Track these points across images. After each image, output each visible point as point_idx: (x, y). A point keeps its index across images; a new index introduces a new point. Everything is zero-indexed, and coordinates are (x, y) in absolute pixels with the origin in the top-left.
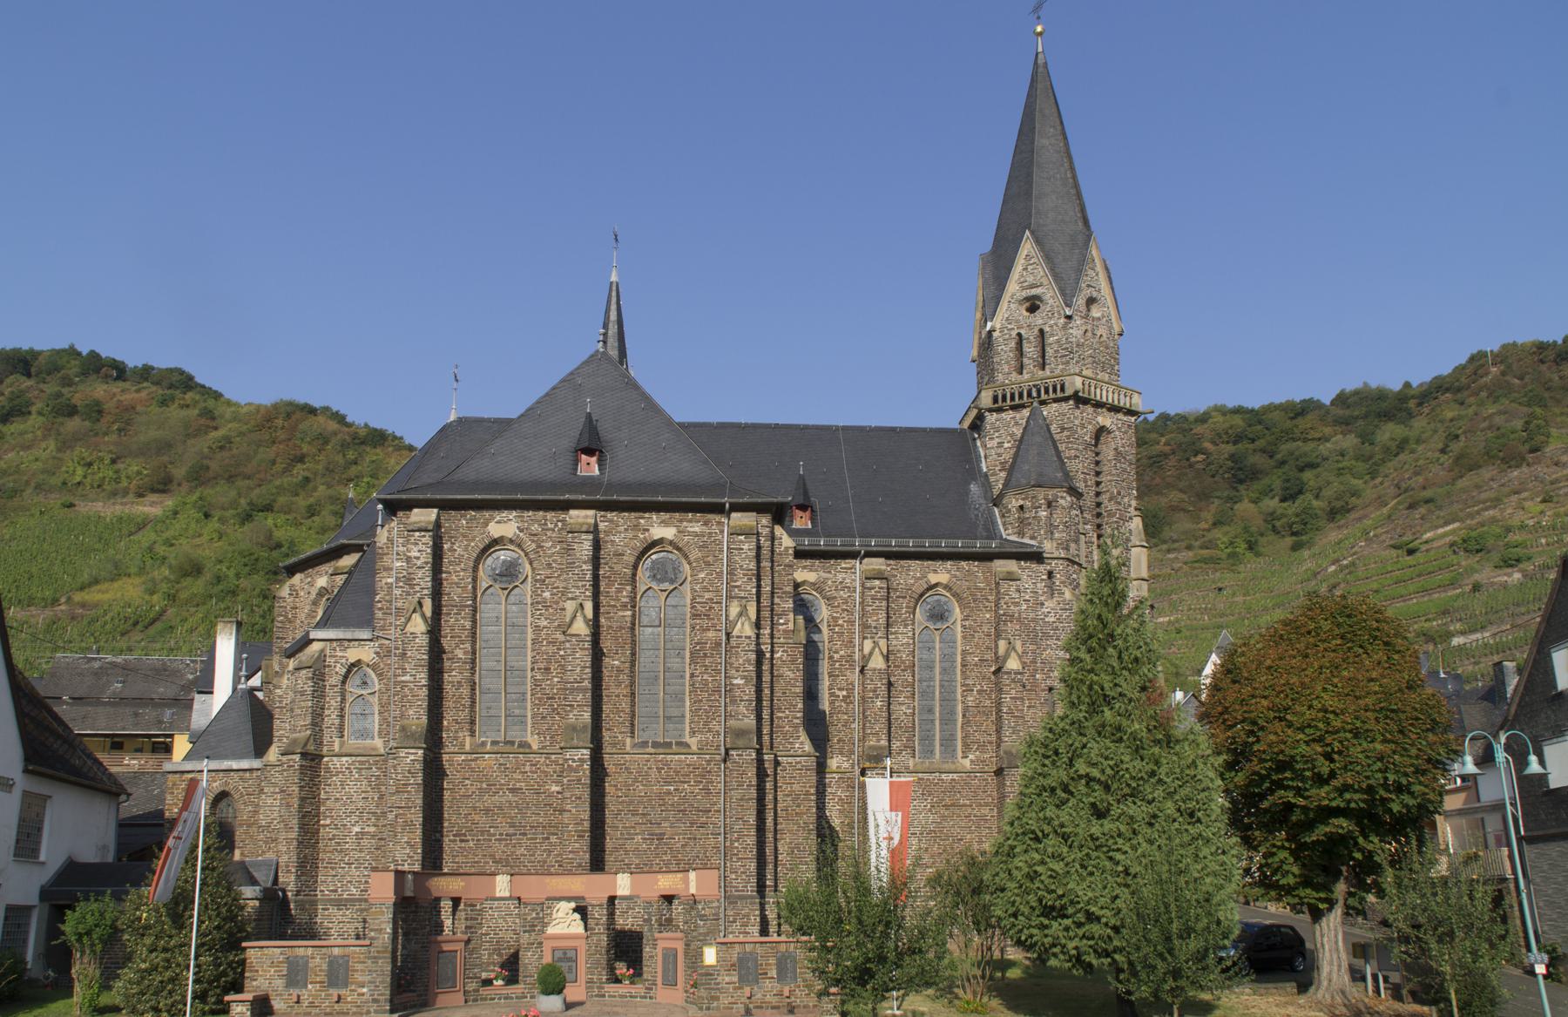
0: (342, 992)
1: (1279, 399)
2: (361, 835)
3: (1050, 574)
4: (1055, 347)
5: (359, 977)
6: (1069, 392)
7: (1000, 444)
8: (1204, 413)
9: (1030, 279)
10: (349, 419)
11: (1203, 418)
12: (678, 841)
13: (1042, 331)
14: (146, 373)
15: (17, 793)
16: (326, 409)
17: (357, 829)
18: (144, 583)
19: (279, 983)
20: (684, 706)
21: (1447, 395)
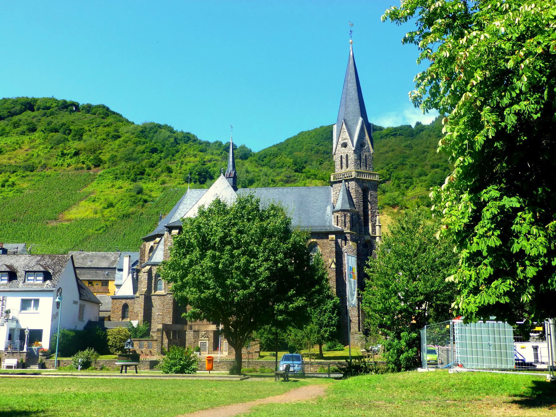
2: (159, 315)
10: (175, 129)
13: (347, 155)
14: (89, 109)
15: (78, 304)
16: (166, 125)
17: (158, 313)
18: (366, 333)
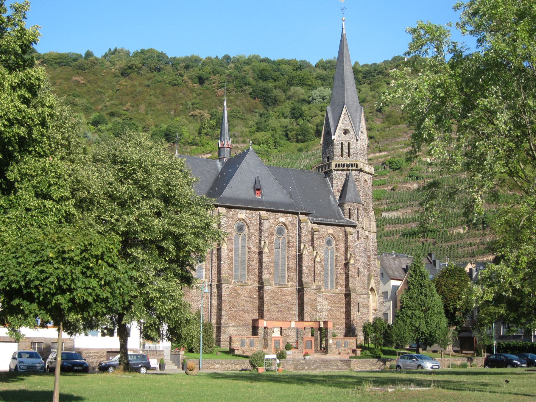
0: (253, 348)
1: (288, 57)
3: (358, 232)
4: (353, 149)
5: (257, 345)
6: (359, 168)
7: (337, 182)
8: (249, 59)
9: (346, 123)
11: (248, 62)
12: (285, 313)
19: (239, 346)
20: (245, 264)
21: (379, 76)
